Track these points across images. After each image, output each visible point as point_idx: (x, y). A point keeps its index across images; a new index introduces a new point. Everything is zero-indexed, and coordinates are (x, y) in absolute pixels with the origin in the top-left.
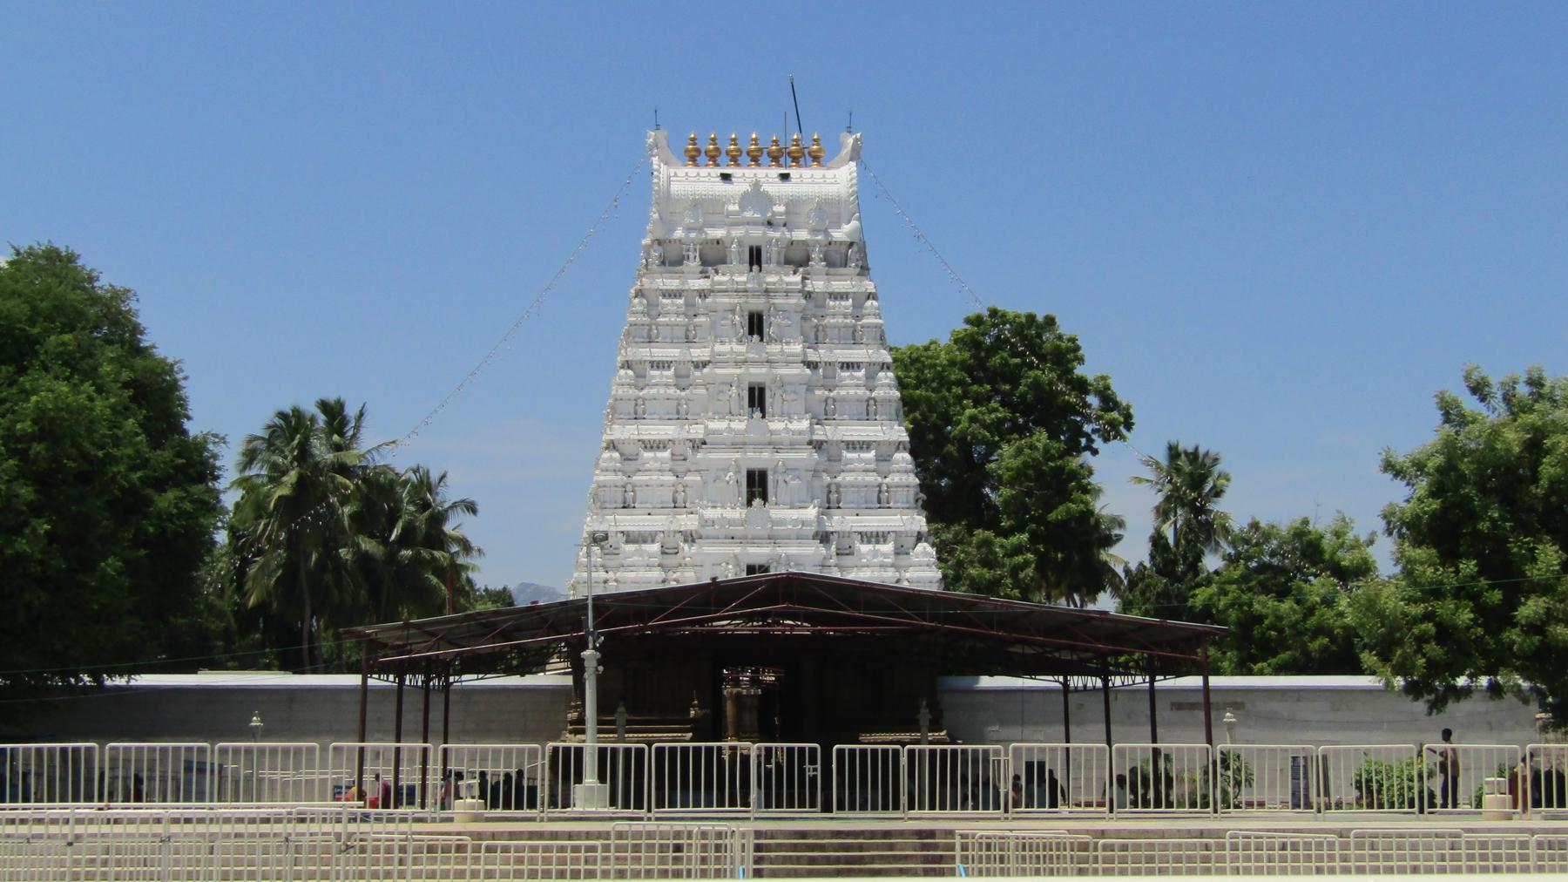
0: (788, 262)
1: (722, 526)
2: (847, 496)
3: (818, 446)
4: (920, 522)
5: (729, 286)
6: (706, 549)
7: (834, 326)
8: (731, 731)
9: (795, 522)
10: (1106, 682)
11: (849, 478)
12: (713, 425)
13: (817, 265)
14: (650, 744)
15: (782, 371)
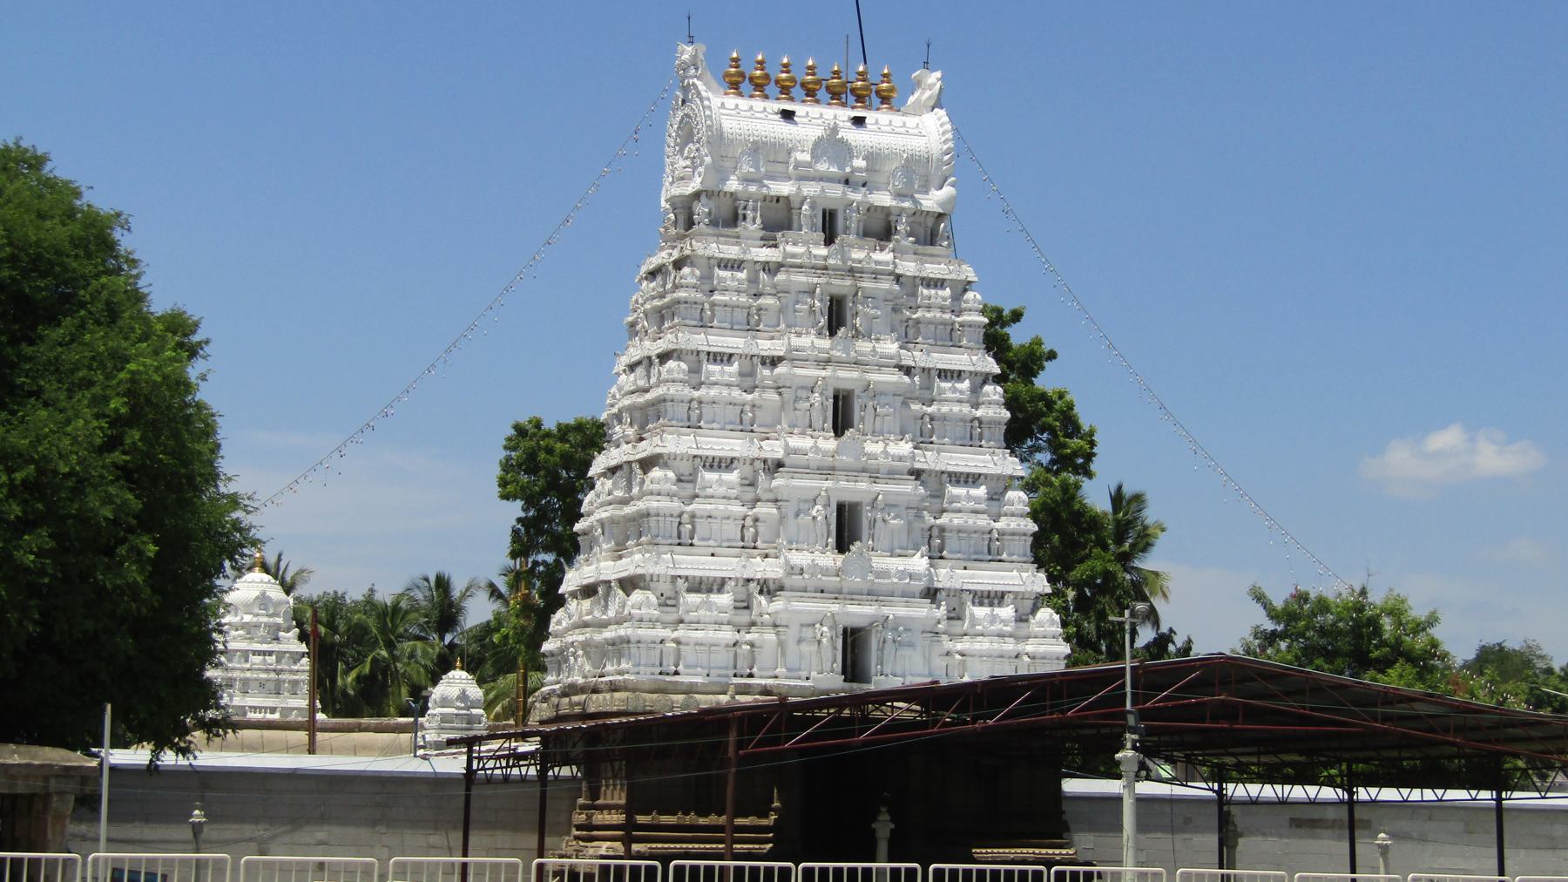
0: (866, 234)
1: (812, 575)
2: (952, 542)
3: (917, 474)
4: (1039, 582)
5: (805, 260)
6: (797, 605)
7: (930, 322)
8: (883, 847)
9: (903, 574)
10: (1351, 794)
11: (957, 520)
12: (796, 442)
13: (903, 240)
14: (665, 859)
15: (875, 377)
